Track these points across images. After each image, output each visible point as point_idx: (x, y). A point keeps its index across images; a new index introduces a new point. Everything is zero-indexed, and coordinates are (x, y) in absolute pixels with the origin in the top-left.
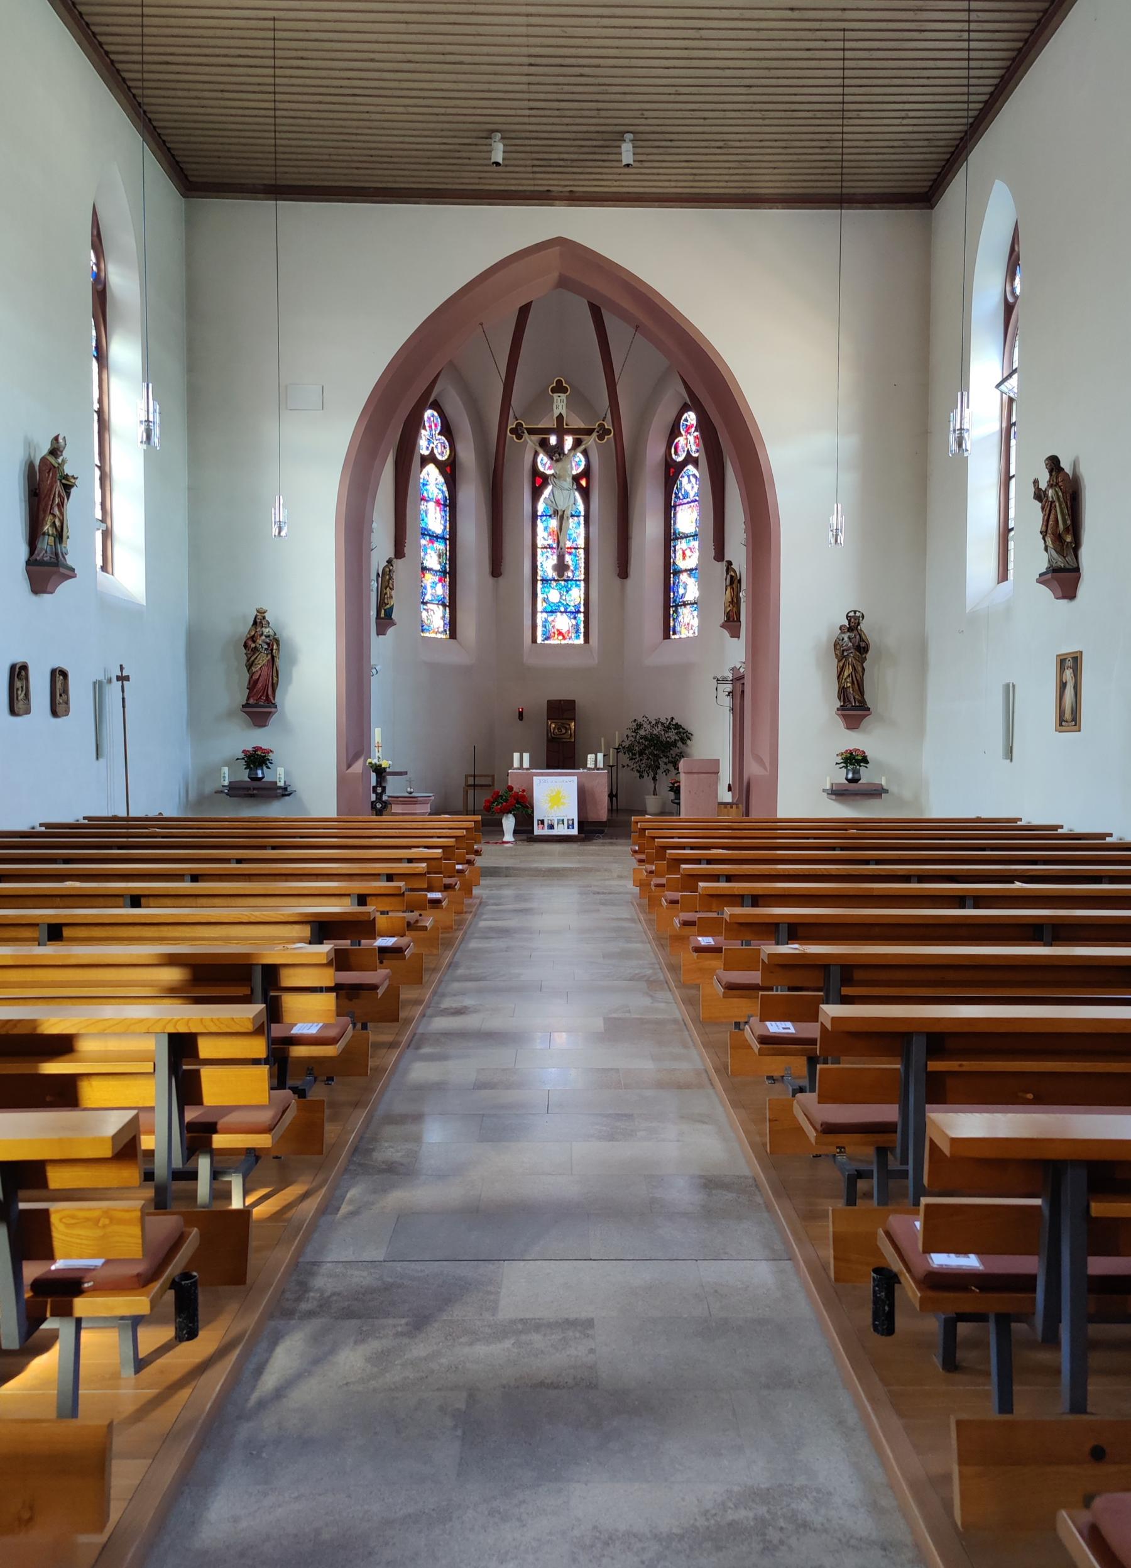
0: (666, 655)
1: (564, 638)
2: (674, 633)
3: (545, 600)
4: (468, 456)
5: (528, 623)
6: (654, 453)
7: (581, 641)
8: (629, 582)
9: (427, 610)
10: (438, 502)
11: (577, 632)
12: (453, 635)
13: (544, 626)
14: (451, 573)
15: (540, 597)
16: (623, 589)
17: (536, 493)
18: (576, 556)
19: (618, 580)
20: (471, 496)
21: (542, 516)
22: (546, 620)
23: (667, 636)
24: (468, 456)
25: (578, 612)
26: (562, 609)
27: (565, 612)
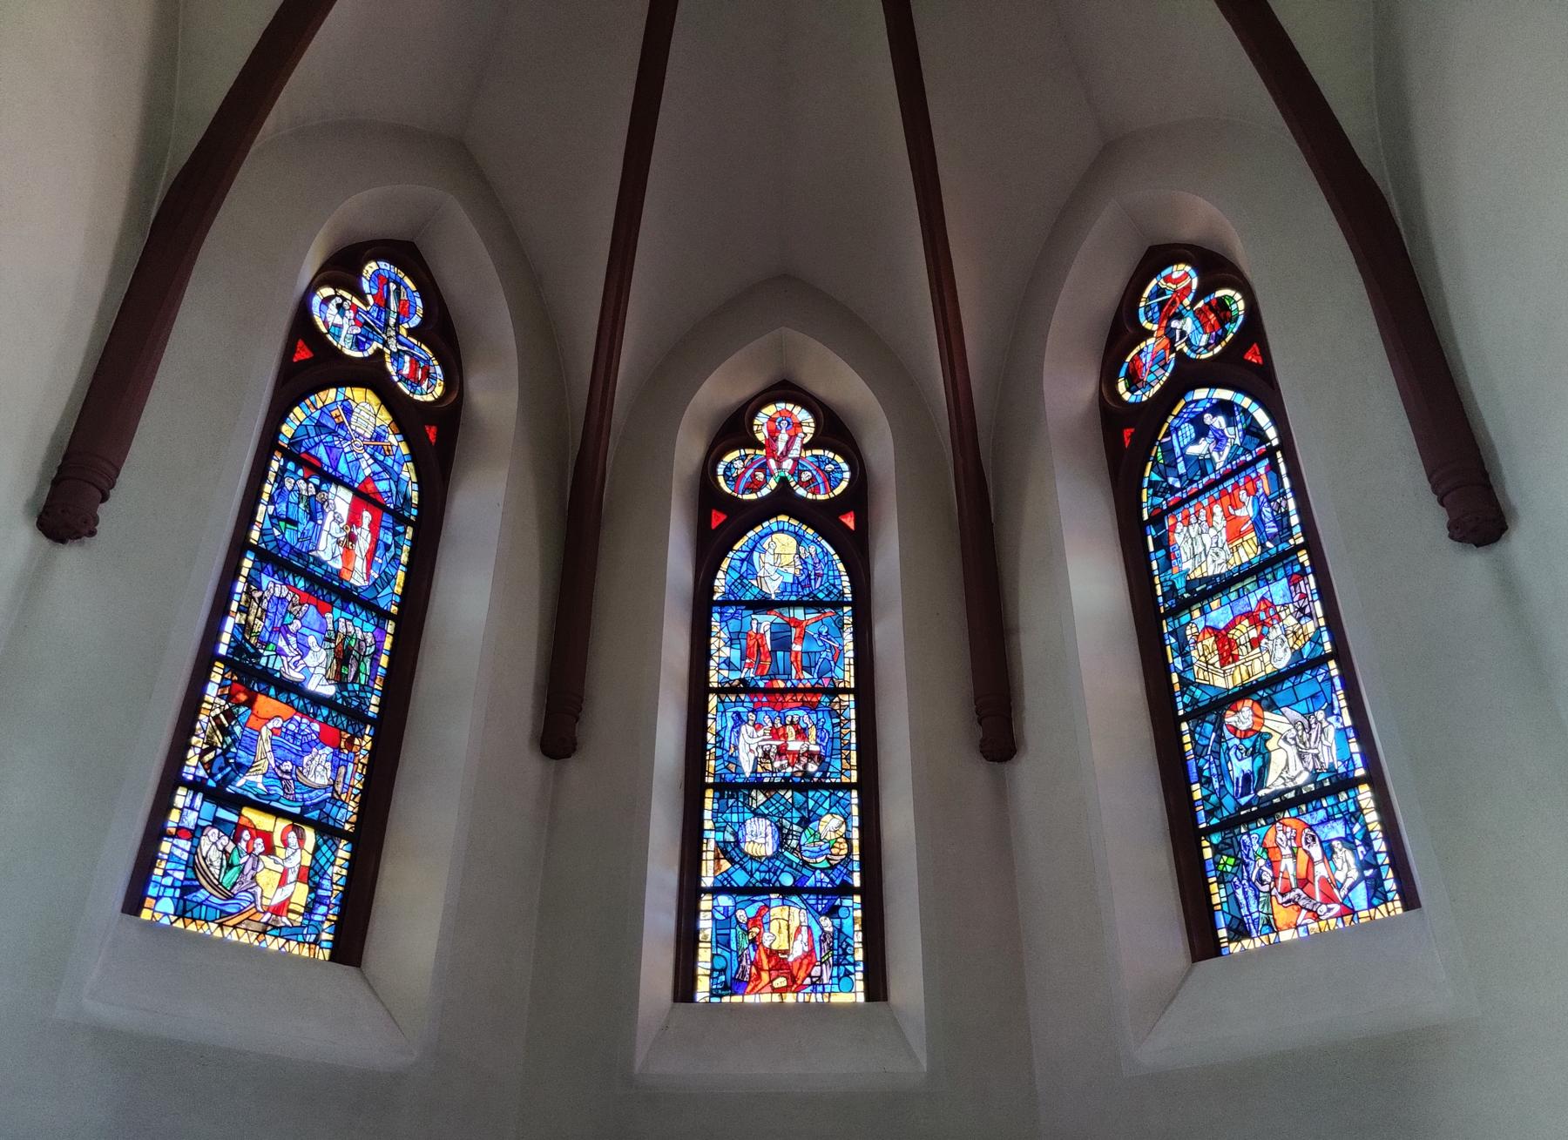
0: (1225, 1016)
1: (794, 984)
2: (1240, 930)
3: (730, 851)
4: (496, 397)
5: (660, 919)
6: (1067, 390)
7: (853, 994)
8: (1026, 770)
9: (235, 832)
10: (364, 497)
11: (841, 959)
12: (349, 945)
13: (722, 941)
14: (384, 724)
15: (711, 839)
16: (1002, 794)
17: (709, 551)
18: (832, 713)
19: (979, 772)
20: (492, 508)
21: (724, 603)
22: (729, 916)
23: (1204, 944)
24: (496, 397)
25: (846, 890)
26: (787, 880)
27: (798, 889)
